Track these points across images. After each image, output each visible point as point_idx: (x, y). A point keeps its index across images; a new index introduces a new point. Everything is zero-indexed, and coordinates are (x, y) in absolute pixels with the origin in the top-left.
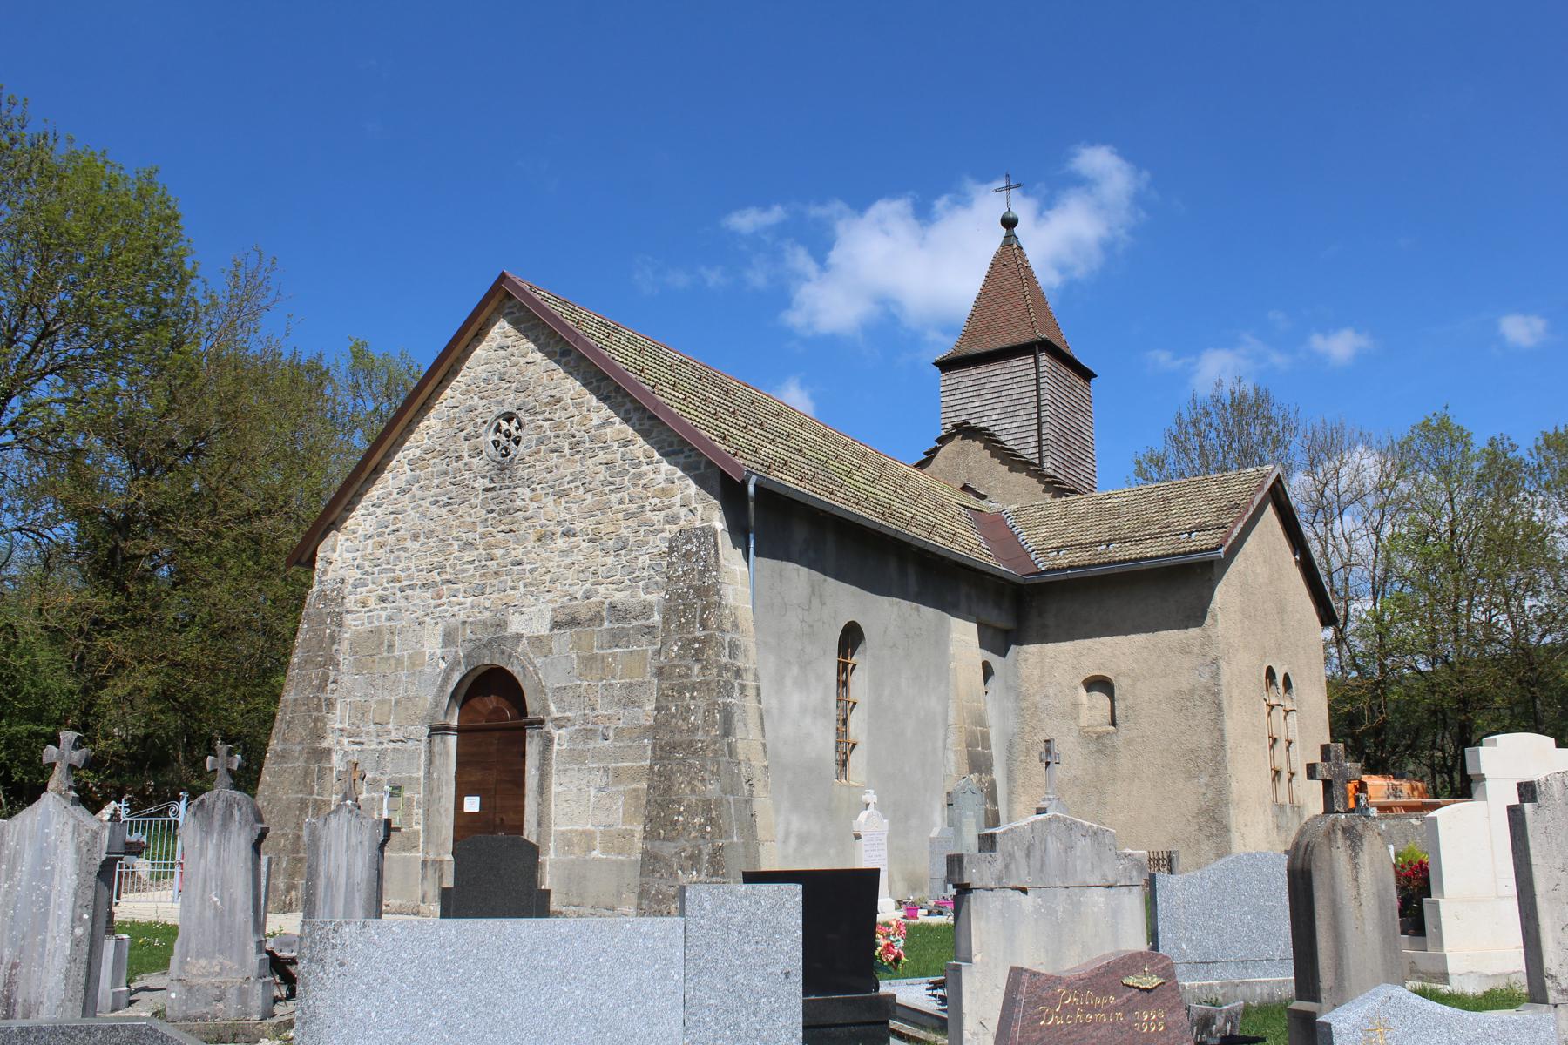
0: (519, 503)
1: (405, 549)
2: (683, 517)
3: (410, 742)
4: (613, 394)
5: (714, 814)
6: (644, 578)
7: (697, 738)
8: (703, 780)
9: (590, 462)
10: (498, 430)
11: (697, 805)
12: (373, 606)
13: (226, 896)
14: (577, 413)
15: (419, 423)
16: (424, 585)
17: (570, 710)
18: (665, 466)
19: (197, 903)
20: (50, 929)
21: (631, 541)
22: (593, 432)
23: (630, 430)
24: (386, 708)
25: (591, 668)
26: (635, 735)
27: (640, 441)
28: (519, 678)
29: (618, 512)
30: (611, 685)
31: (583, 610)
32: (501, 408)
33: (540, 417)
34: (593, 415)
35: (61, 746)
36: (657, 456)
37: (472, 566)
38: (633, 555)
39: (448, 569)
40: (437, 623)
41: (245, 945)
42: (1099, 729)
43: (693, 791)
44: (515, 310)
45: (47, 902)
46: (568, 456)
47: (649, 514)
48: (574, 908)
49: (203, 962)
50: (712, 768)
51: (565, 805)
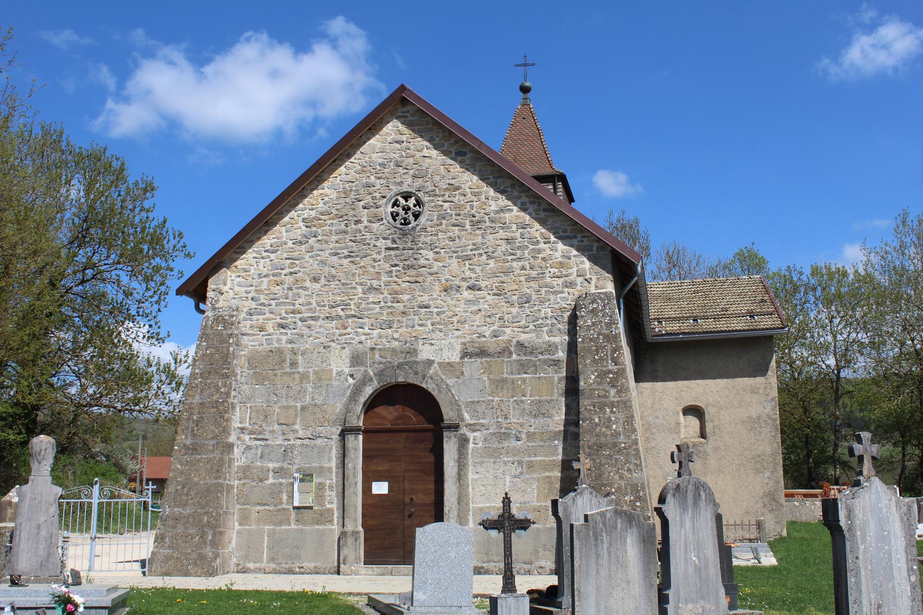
0: (422, 262)
1: (306, 289)
2: (579, 284)
3: (320, 440)
4: (510, 189)
5: (641, 493)
6: (547, 325)
7: (620, 441)
8: (629, 470)
9: (491, 237)
10: (395, 204)
11: (626, 488)
12: (271, 331)
13: (701, 556)
14: (475, 200)
15: (313, 190)
16: (327, 318)
17: (484, 418)
18: (560, 246)
19: (682, 562)
20: (896, 578)
21: (534, 297)
22: (492, 215)
23: (528, 217)
24: (292, 412)
25: (502, 388)
26: (545, 438)
27: (537, 226)
28: (435, 393)
29: (520, 275)
30: (522, 402)
31: (492, 345)
32: (399, 188)
33: (441, 199)
34: (492, 203)
35: (864, 442)
36: (553, 238)
37: (378, 306)
38: (536, 308)
39: (353, 307)
40: (343, 348)
41: (717, 592)
42: (693, 440)
43: (621, 477)
44: (408, 115)
45: (890, 559)
46: (469, 231)
47: (549, 280)
48: (494, 564)
49: (690, 606)
50: (636, 462)
51: (482, 488)
